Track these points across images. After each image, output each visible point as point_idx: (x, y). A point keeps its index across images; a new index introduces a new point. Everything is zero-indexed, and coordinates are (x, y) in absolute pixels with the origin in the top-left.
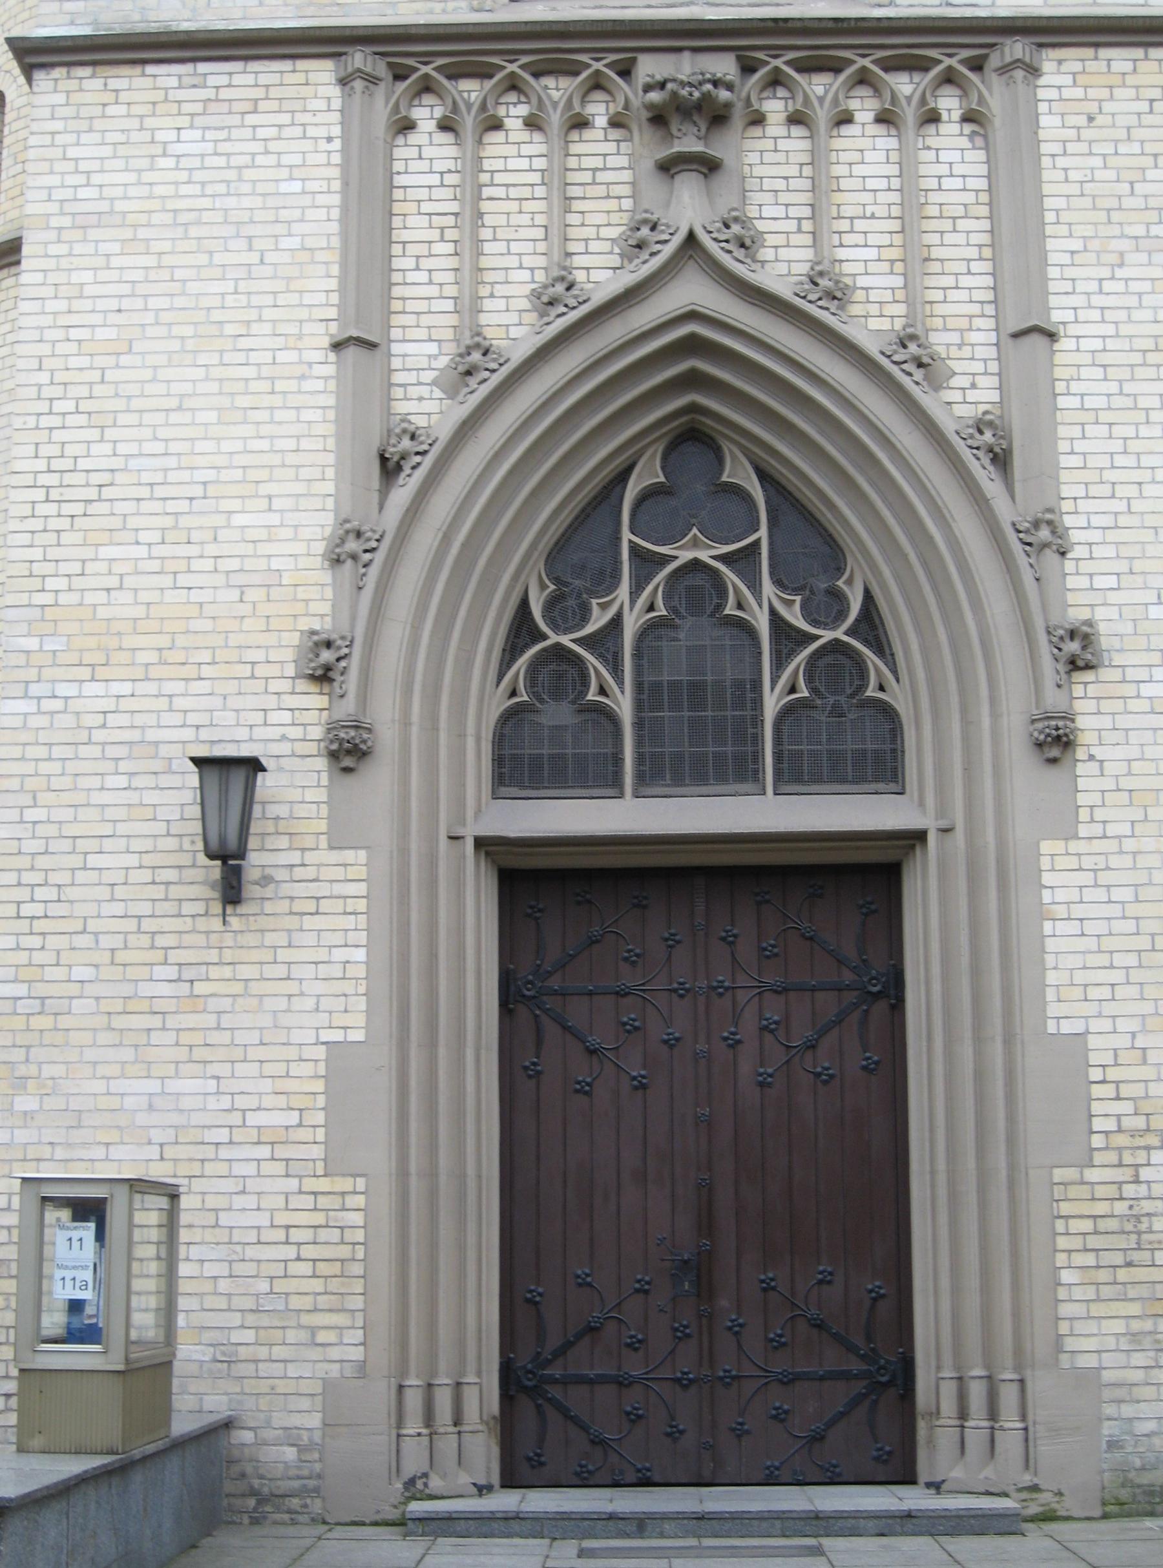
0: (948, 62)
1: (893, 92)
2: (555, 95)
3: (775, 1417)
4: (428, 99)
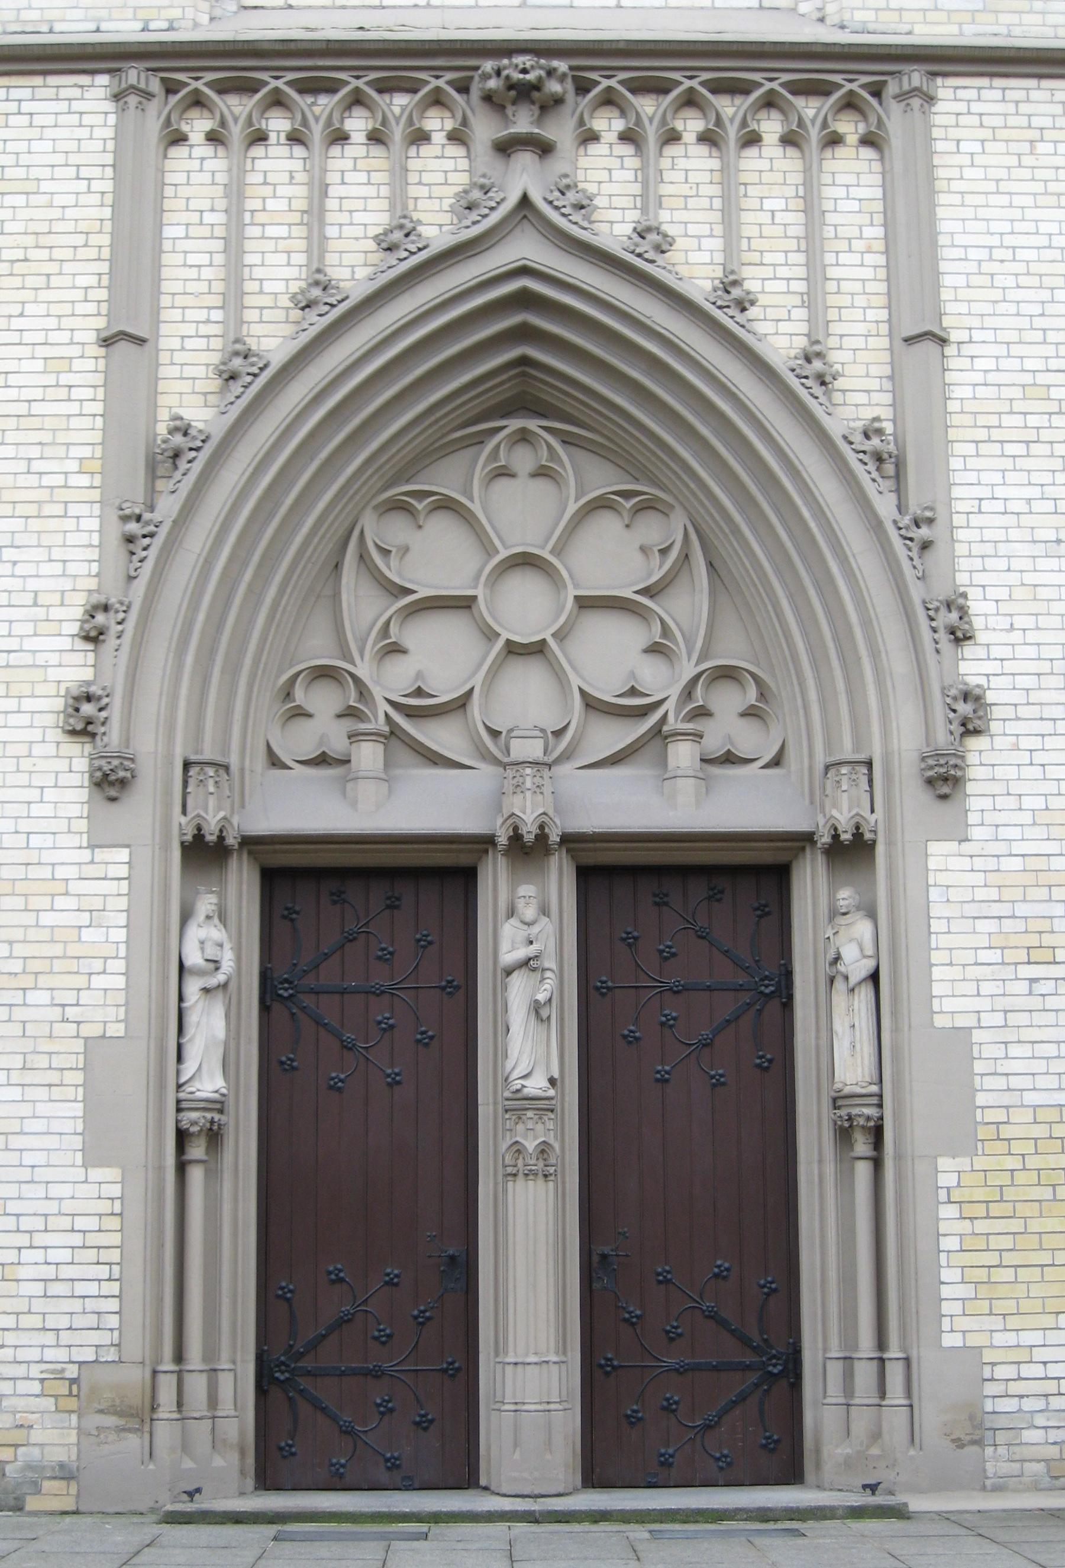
0: (274, 84)
1: (637, 114)
2: (237, 110)
3: (664, 1408)
4: (358, 112)
